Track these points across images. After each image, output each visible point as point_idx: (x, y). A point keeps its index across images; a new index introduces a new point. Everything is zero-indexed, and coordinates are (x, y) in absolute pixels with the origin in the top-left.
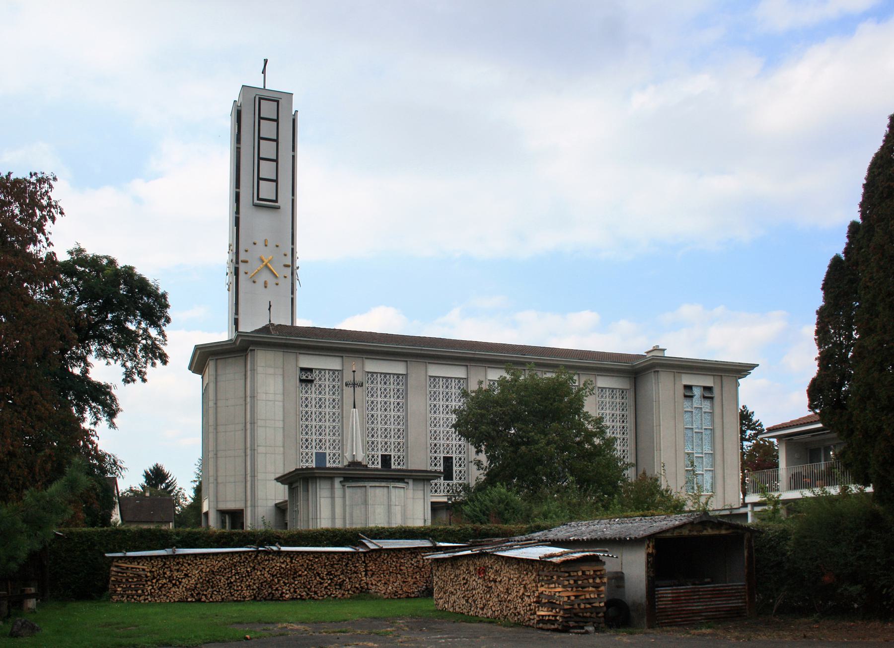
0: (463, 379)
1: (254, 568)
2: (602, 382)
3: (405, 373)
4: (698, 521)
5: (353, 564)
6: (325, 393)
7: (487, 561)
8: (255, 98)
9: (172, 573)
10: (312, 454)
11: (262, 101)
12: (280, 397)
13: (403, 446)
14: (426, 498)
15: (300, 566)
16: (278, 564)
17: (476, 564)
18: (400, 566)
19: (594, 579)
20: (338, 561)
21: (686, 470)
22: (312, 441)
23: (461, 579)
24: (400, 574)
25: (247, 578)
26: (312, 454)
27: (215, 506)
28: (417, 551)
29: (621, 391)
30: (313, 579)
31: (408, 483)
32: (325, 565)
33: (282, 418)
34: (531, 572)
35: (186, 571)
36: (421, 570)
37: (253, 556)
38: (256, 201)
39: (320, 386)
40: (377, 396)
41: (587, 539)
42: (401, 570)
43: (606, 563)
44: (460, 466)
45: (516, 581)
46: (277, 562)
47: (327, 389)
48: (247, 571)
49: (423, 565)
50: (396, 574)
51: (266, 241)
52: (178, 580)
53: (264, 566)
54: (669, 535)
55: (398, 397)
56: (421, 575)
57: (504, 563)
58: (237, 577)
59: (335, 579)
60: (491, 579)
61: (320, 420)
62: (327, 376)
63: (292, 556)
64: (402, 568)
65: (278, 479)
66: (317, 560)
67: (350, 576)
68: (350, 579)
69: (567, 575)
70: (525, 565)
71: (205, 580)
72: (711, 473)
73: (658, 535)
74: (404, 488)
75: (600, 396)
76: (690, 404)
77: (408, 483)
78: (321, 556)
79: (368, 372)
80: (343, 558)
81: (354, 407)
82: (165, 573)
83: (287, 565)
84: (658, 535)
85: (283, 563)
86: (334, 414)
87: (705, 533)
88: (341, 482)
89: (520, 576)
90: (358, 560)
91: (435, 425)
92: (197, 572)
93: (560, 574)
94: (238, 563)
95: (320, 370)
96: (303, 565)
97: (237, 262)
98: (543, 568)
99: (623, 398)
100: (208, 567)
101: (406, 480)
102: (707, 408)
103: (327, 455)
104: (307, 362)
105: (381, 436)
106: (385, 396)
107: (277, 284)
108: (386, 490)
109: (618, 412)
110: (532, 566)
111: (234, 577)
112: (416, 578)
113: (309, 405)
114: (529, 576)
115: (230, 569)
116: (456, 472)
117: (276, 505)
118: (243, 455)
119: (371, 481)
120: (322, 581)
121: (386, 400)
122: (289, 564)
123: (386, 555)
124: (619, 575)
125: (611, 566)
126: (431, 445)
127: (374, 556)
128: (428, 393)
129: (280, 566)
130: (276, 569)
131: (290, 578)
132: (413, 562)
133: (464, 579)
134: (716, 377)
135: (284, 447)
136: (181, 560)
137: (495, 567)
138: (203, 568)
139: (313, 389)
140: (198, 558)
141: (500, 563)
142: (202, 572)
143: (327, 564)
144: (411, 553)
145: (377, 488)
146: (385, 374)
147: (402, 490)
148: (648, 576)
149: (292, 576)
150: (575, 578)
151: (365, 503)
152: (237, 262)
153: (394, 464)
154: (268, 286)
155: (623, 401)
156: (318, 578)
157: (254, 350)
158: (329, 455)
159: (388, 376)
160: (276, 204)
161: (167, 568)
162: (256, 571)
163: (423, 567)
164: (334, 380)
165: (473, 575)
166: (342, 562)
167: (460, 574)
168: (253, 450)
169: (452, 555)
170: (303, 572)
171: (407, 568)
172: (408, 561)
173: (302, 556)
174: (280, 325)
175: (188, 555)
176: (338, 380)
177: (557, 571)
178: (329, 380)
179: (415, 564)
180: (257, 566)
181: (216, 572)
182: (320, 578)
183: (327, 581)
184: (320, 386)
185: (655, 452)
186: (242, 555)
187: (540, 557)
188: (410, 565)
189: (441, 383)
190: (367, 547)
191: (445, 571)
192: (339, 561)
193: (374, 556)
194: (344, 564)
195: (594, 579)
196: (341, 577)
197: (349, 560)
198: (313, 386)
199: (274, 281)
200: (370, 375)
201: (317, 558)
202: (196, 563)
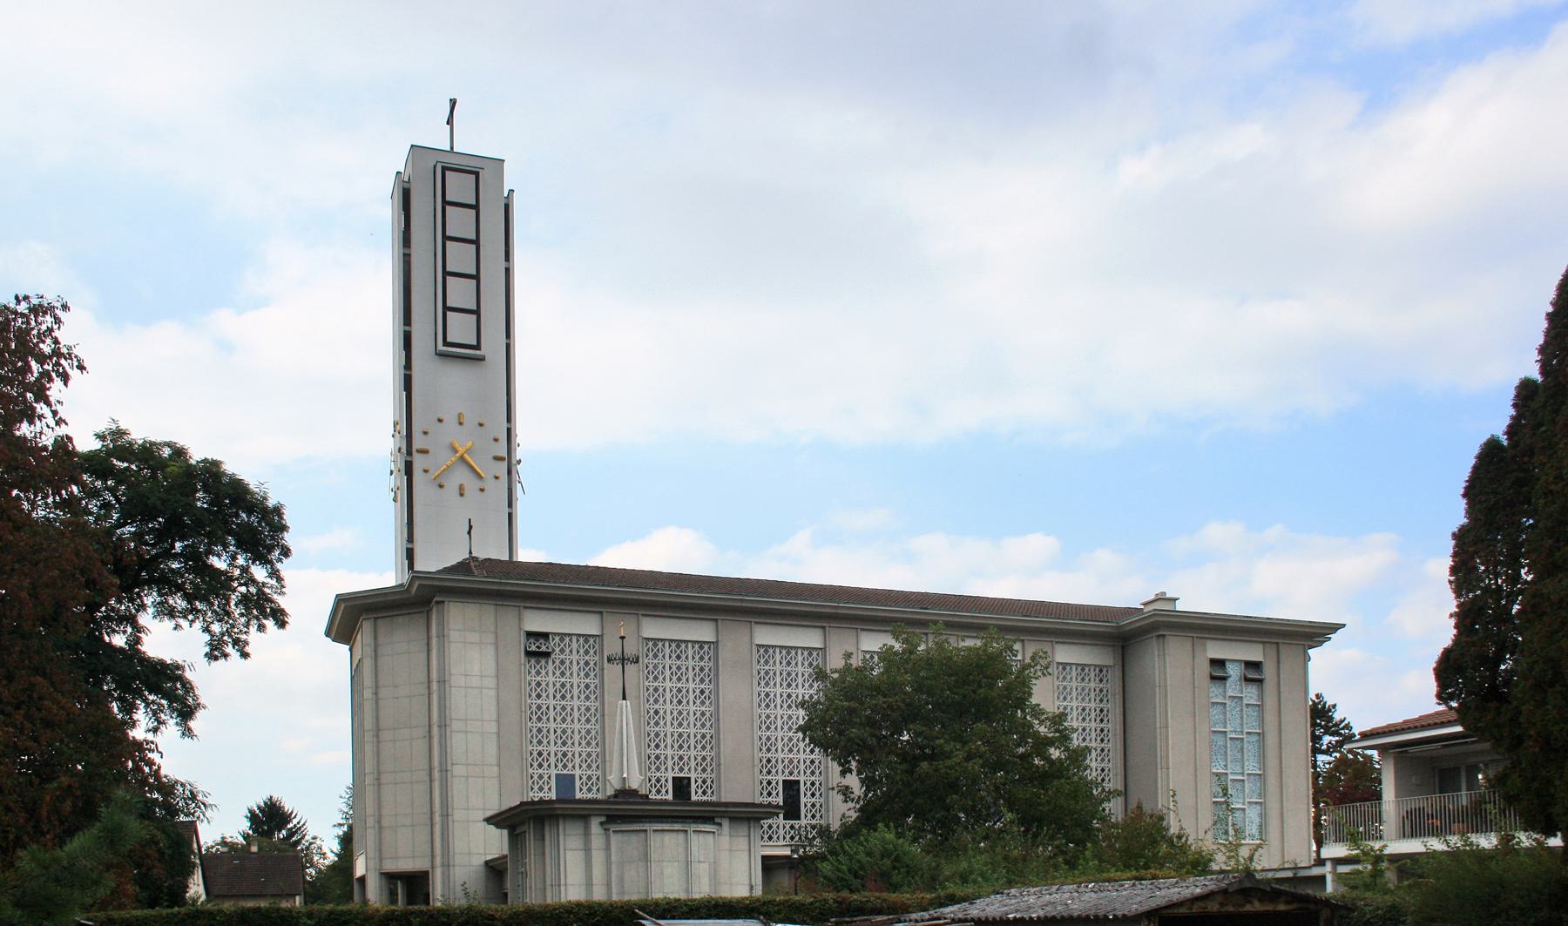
0: (816, 649)
4: (1235, 887)
8: (435, 167)
11: (447, 173)
12: (491, 682)
14: (752, 850)
21: (1214, 802)
22: (549, 754)
26: (549, 778)
29: (1097, 670)
31: (720, 825)
33: (494, 717)
38: (441, 347)
39: (562, 662)
41: (1038, 917)
47: (575, 668)
61: (564, 720)
65: (489, 820)
74: (714, 833)
76: (1221, 690)
77: (720, 825)
81: (624, 698)
84: (1164, 912)
87: (1248, 908)
95: (562, 636)
97: (409, 453)
99: (1101, 681)
101: (717, 820)
102: (1251, 698)
104: (537, 621)
106: (679, 679)
107: (482, 490)
108: (681, 836)
109: (1093, 705)
113: (544, 695)
116: (806, 806)
117: (487, 863)
118: (427, 779)
119: (655, 822)
121: (679, 685)
128: (755, 673)
134: (1267, 645)
135: (499, 765)
139: (551, 667)
145: (665, 833)
146: (679, 642)
147: (711, 836)
151: (646, 858)
152: (409, 453)
153: (696, 793)
154: (466, 493)
157: (443, 602)
158: (581, 779)
160: (478, 352)
168: (444, 771)
184: (562, 662)
185: (1159, 771)
198: (550, 662)
199: (480, 484)
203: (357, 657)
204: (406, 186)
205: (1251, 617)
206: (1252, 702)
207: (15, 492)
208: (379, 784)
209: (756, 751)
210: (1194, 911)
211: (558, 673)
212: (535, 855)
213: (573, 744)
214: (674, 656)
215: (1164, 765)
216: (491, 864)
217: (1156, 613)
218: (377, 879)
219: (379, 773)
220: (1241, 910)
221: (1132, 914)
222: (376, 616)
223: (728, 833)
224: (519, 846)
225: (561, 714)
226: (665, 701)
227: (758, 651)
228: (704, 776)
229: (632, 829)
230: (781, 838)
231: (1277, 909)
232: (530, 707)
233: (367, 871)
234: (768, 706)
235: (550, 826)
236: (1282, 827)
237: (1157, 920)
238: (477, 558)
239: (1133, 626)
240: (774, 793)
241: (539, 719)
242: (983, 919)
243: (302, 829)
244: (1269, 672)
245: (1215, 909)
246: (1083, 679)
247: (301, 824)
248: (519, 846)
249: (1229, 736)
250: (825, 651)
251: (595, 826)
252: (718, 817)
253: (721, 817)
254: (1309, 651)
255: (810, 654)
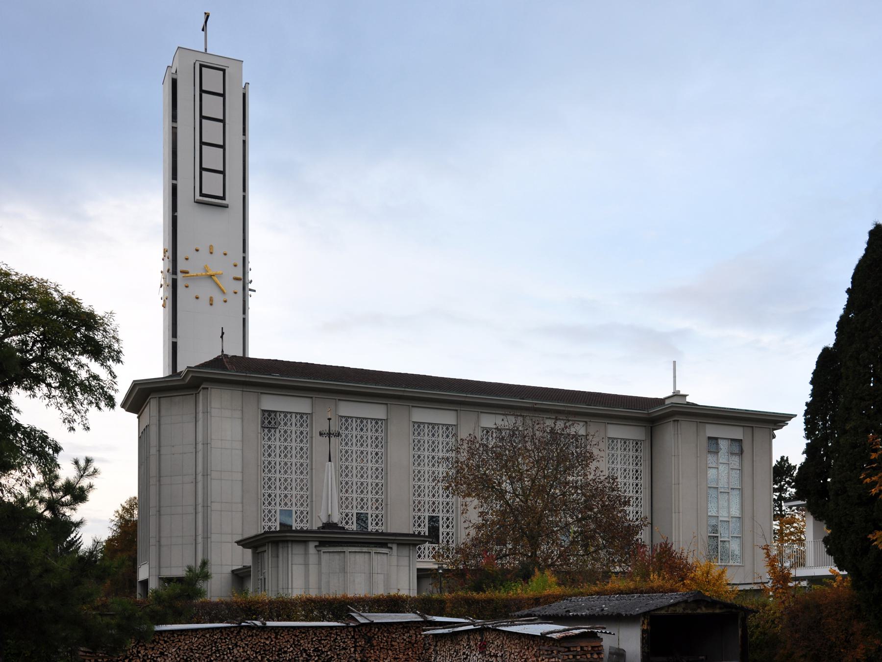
0: (452, 425)
1: (236, 645)
2: (616, 431)
3: (385, 418)
4: (692, 599)
5: (341, 639)
6: (291, 440)
7: (488, 637)
8: (195, 64)
9: (147, 651)
10: (275, 512)
11: (203, 69)
13: (379, 504)
14: (411, 566)
15: (286, 642)
16: (262, 641)
17: (477, 639)
18: (391, 641)
19: (592, 654)
20: (326, 637)
21: (709, 536)
22: (275, 496)
23: (462, 653)
24: (391, 650)
25: (229, 655)
26: (275, 512)
27: (157, 574)
28: (410, 625)
29: (635, 443)
30: (299, 656)
31: (391, 548)
32: (312, 641)
33: (240, 470)
34: (532, 647)
35: (162, 649)
36: (413, 645)
37: (236, 632)
38: (198, 197)
39: (285, 432)
40: (352, 444)
41: (586, 615)
42: (392, 646)
43: (603, 639)
44: (448, 527)
45: (517, 656)
46: (261, 638)
47: (294, 436)
48: (229, 649)
49: (416, 641)
50: (387, 650)
51: (211, 247)
52: (153, 659)
53: (247, 643)
54: (663, 612)
55: (377, 446)
56: (413, 651)
57: (505, 638)
58: (218, 655)
59: (323, 656)
60: (492, 654)
61: (286, 472)
62: (294, 420)
63: (277, 631)
64: (393, 643)
65: (238, 543)
66: (303, 635)
67: (338, 652)
68: (338, 655)
69: (566, 650)
70: (526, 640)
71: (183, 659)
72: (738, 540)
73: (653, 613)
74: (387, 554)
75: (610, 448)
76: (715, 458)
77: (391, 548)
78: (308, 631)
79: (342, 417)
80: (331, 633)
81: (330, 461)
82: (139, 652)
83: (272, 641)
84: (653, 613)
85: (267, 639)
86: (302, 465)
87: (699, 611)
88: (316, 546)
89: (521, 651)
90: (347, 635)
91: (419, 479)
92: (174, 650)
93: (560, 649)
94: (219, 640)
95: (286, 413)
96: (288, 641)
97: (175, 272)
98: (544, 643)
99: (637, 450)
100: (186, 644)
101: (389, 545)
102: (734, 464)
103: (294, 513)
104: (271, 403)
105: (357, 492)
106: (362, 445)
107: (225, 301)
108: (367, 556)
109: (631, 467)
110: (533, 641)
111: (214, 654)
112: (408, 654)
113: (273, 455)
114: (530, 651)
115: (210, 646)
116: (443, 534)
117: (233, 571)
118: (193, 511)
120: (309, 658)
121: (362, 449)
122: (274, 640)
123: (377, 629)
124: (621, 652)
125: (608, 642)
126: (414, 502)
127: (364, 630)
128: (411, 441)
129: (264, 642)
130: (259, 646)
131: (274, 655)
132: (405, 638)
133: (464, 653)
134: (745, 428)
135: (242, 503)
136: (157, 637)
137: (496, 643)
138: (180, 646)
139: (278, 435)
140: (176, 635)
141: (502, 638)
142: (180, 649)
143: (314, 639)
144: (404, 628)
145: (357, 554)
146: (362, 419)
147: (385, 556)
148: (643, 652)
149: (277, 653)
150: (575, 653)
151: (344, 570)
152: (175, 272)
153: (372, 524)
154: (214, 303)
155: (637, 454)
156: (304, 655)
158: (296, 513)
159: (365, 422)
161: (141, 646)
162: (238, 648)
163: (416, 642)
164: (302, 425)
165: (473, 650)
166: (330, 637)
167: (460, 649)
168: (206, 506)
169: (451, 630)
170: (288, 648)
171: (398, 643)
172: (400, 636)
173: (288, 631)
174: (235, 356)
175: (165, 631)
176: (307, 425)
177: (557, 646)
178: (296, 425)
179: (407, 640)
180: (239, 642)
181: (195, 649)
182: (307, 655)
183: (314, 657)
184: (285, 432)
185: (674, 514)
186: (223, 630)
187: (541, 633)
188: (402, 641)
189: (426, 430)
190: (357, 620)
191: (444, 646)
192: (327, 636)
193: (364, 630)
194: (332, 639)
195: (592, 654)
196: (329, 653)
197: (337, 635)
198: (277, 431)
199: (223, 298)
200: (344, 420)
201: (303, 633)
202: (173, 640)
203: (145, 423)
204: (175, 77)
205: (735, 409)
206: (735, 467)
207: (68, 378)
208: (160, 515)
209: (411, 495)
210: (669, 612)
211: (282, 439)
212: (271, 568)
213: (291, 489)
214: (359, 429)
215: (677, 511)
216: (236, 573)
217: (674, 405)
218: (157, 581)
219: (160, 507)
220: (695, 612)
221: (635, 614)
222: (159, 396)
223: (396, 554)
224: (260, 561)
225: (284, 468)
226: (352, 460)
227: (414, 426)
228: (377, 512)
229: (335, 550)
230: (427, 556)
231: (715, 612)
232: (264, 463)
233: (149, 576)
234: (419, 464)
235: (283, 547)
236: (754, 554)
237: (649, 617)
238: (227, 355)
239: (655, 415)
240: (423, 525)
241: (270, 471)
242: (552, 615)
243: (78, 542)
244: (746, 447)
245: (681, 612)
246: (625, 449)
247: (76, 538)
248: (260, 564)
249: (719, 491)
250: (457, 427)
251: (312, 546)
252: (390, 543)
253: (392, 543)
254: (774, 431)
255: (447, 429)
